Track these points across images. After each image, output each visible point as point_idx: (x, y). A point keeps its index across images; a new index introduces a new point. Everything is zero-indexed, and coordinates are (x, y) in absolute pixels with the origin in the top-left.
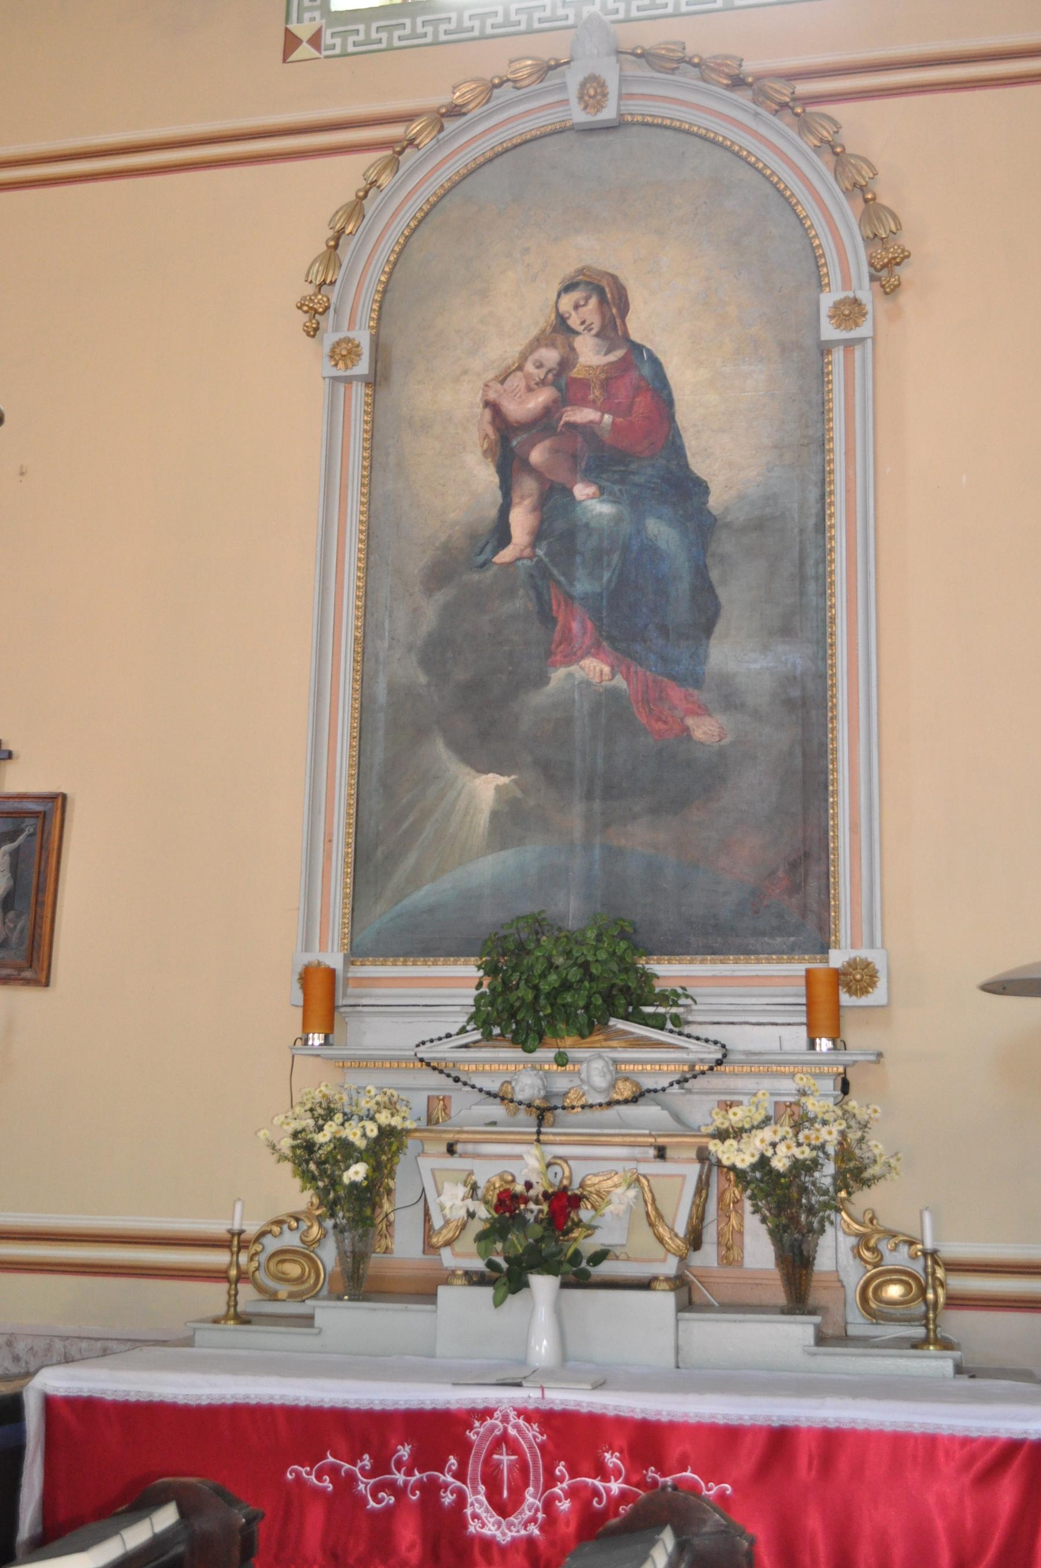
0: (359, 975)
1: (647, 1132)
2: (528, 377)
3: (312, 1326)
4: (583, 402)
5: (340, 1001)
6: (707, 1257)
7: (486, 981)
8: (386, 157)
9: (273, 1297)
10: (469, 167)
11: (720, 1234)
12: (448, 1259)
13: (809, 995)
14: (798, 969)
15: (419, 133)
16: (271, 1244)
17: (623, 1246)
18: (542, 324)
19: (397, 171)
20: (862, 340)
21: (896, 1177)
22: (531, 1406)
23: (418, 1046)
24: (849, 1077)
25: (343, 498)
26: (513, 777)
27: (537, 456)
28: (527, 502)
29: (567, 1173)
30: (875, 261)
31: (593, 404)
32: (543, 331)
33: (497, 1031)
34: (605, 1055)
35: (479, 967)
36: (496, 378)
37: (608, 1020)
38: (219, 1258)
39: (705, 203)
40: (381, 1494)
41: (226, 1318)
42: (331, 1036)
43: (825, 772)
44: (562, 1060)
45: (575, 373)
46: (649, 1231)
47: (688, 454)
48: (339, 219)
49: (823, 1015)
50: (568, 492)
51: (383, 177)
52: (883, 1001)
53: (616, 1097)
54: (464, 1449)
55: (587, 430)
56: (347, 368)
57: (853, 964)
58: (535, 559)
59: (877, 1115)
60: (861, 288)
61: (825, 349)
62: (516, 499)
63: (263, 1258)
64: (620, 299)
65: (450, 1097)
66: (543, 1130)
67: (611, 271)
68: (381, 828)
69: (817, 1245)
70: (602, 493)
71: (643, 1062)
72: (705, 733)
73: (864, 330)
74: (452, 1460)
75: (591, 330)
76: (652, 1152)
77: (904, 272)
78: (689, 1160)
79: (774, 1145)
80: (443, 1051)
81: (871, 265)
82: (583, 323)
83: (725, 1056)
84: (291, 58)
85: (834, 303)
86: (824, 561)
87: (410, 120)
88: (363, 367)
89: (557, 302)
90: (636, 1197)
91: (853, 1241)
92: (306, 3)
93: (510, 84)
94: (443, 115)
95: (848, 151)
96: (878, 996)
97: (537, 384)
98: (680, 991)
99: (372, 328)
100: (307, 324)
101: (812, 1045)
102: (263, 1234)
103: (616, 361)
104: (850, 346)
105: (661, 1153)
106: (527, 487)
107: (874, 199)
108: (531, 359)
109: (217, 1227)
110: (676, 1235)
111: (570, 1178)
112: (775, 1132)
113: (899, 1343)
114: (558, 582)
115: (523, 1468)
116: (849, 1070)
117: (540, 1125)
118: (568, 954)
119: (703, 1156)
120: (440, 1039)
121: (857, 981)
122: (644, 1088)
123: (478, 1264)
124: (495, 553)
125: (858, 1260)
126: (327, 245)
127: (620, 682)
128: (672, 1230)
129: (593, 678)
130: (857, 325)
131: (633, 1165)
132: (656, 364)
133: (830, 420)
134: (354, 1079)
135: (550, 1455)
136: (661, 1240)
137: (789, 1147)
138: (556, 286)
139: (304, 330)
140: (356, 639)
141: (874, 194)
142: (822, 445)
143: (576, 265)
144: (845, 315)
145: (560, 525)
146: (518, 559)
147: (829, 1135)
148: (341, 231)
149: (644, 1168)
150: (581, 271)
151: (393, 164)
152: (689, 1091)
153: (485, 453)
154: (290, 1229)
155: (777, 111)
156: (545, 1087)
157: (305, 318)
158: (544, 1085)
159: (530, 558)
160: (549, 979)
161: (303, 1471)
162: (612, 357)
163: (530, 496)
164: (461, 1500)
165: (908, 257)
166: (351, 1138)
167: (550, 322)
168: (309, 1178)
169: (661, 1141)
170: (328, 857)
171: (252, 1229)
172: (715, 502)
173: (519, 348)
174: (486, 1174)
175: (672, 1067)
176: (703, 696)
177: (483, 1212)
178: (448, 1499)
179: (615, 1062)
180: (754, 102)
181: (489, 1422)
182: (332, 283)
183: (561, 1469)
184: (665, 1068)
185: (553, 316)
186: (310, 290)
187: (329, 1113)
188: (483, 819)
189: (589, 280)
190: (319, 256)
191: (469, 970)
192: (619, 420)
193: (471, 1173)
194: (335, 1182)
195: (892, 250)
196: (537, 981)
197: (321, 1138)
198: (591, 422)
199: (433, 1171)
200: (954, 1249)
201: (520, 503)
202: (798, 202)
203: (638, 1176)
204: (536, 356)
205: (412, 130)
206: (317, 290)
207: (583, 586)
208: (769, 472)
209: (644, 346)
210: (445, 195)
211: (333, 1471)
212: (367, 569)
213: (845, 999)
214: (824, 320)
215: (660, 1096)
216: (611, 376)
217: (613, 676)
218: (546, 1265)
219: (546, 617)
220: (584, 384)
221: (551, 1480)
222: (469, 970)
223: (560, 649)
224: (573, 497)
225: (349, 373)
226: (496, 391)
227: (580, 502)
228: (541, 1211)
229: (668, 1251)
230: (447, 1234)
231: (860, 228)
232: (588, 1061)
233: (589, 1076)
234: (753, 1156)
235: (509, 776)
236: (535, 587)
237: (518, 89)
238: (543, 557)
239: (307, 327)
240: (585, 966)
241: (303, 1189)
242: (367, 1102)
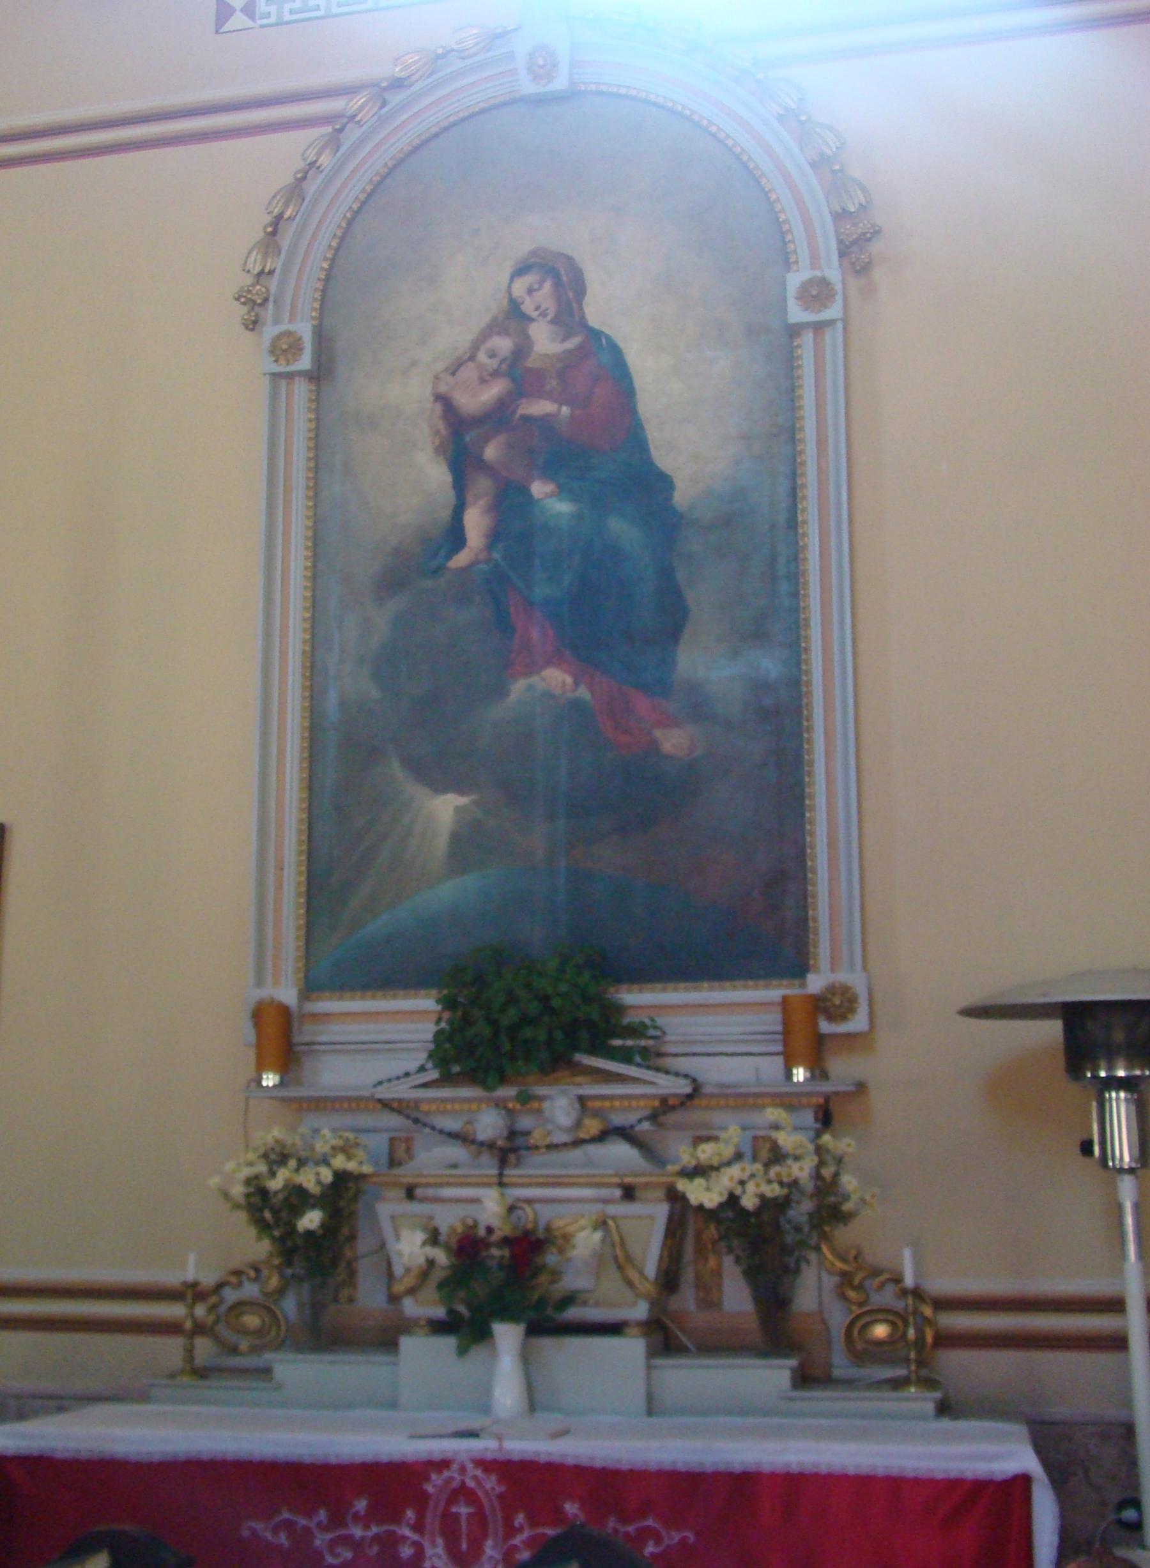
2: (481, 367)
3: (271, 1380)
5: (297, 1039)
6: (686, 1299)
7: (446, 1015)
9: (234, 1350)
10: (414, 144)
11: (698, 1276)
12: (410, 1307)
14: (774, 993)
16: (231, 1296)
19: (337, 151)
20: (832, 322)
22: (489, 1456)
23: (375, 1086)
25: (287, 502)
27: (491, 452)
32: (495, 319)
33: (456, 1069)
35: (438, 1001)
36: (446, 370)
38: (174, 1311)
40: (339, 1550)
41: (182, 1372)
45: (531, 363)
46: (618, 1275)
47: (652, 447)
48: (277, 204)
50: (524, 491)
53: (582, 1135)
54: (421, 1501)
55: (545, 423)
57: (831, 990)
62: (469, 498)
63: (223, 1309)
66: (507, 1172)
71: (611, 1098)
73: (834, 311)
74: (410, 1514)
76: (618, 1193)
79: (742, 1183)
80: (401, 1091)
82: (537, 309)
86: (796, 559)
88: (305, 362)
89: (509, 287)
90: (603, 1241)
91: (836, 1279)
94: (385, 89)
96: (858, 1023)
98: (647, 1021)
99: (313, 318)
100: (245, 317)
101: (789, 1075)
102: (220, 1286)
105: (629, 1193)
106: (482, 487)
108: (483, 348)
109: (172, 1278)
110: (646, 1279)
112: (743, 1170)
113: (880, 1384)
115: (480, 1518)
118: (528, 985)
119: (675, 1197)
123: (440, 1312)
124: (449, 556)
126: (265, 232)
127: (584, 693)
130: (826, 307)
131: (599, 1207)
133: (801, 408)
134: (312, 1120)
135: (508, 1505)
136: (630, 1284)
137: (758, 1185)
139: (244, 324)
140: (304, 652)
147: (802, 1170)
148: (279, 217)
149: (611, 1209)
150: (534, 253)
152: (661, 1126)
154: (249, 1279)
157: (244, 309)
161: (259, 1526)
162: (570, 344)
164: (419, 1554)
166: (306, 1185)
168: (263, 1227)
170: (279, 886)
171: (209, 1279)
172: (681, 498)
174: (448, 1219)
175: (642, 1103)
177: (441, 1256)
178: (406, 1552)
179: (582, 1099)
181: (446, 1474)
182: (271, 272)
183: (520, 1519)
184: (634, 1103)
185: (505, 302)
186: (249, 280)
187: (283, 1159)
188: (441, 844)
191: (427, 1003)
192: (578, 412)
194: (291, 1231)
195: (861, 225)
197: (275, 1184)
198: (548, 415)
199: (393, 1217)
200: (942, 1284)
205: (353, 106)
207: (542, 591)
211: (288, 1525)
212: (315, 577)
213: (825, 1027)
216: (569, 364)
218: (507, 1314)
219: (503, 624)
220: (539, 375)
221: (511, 1531)
222: (427, 1003)
224: (531, 496)
227: (539, 500)
228: (503, 1257)
229: (637, 1295)
230: (409, 1282)
239: (245, 319)
240: (545, 999)
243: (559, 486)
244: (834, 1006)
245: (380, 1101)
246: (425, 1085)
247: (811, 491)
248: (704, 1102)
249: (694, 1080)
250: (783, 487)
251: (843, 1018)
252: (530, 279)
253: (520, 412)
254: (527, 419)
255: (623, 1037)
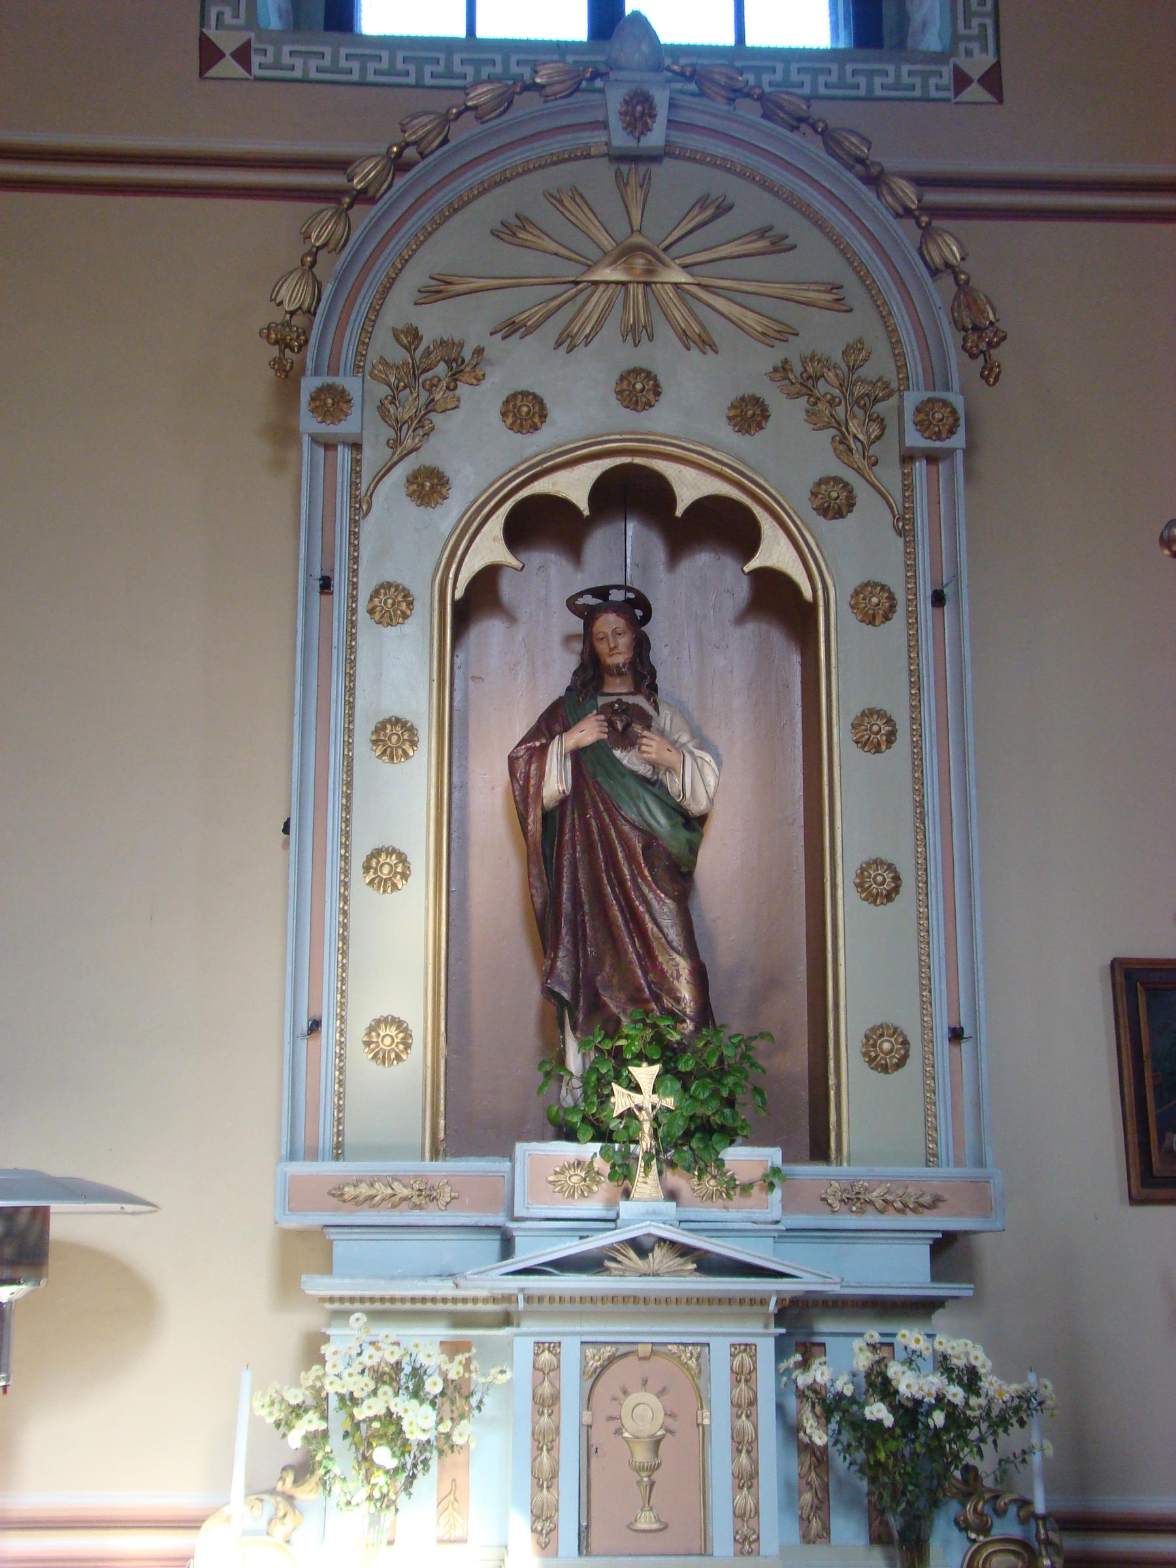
20: (950, 452)
92: (974, 5)
214: (909, 426)
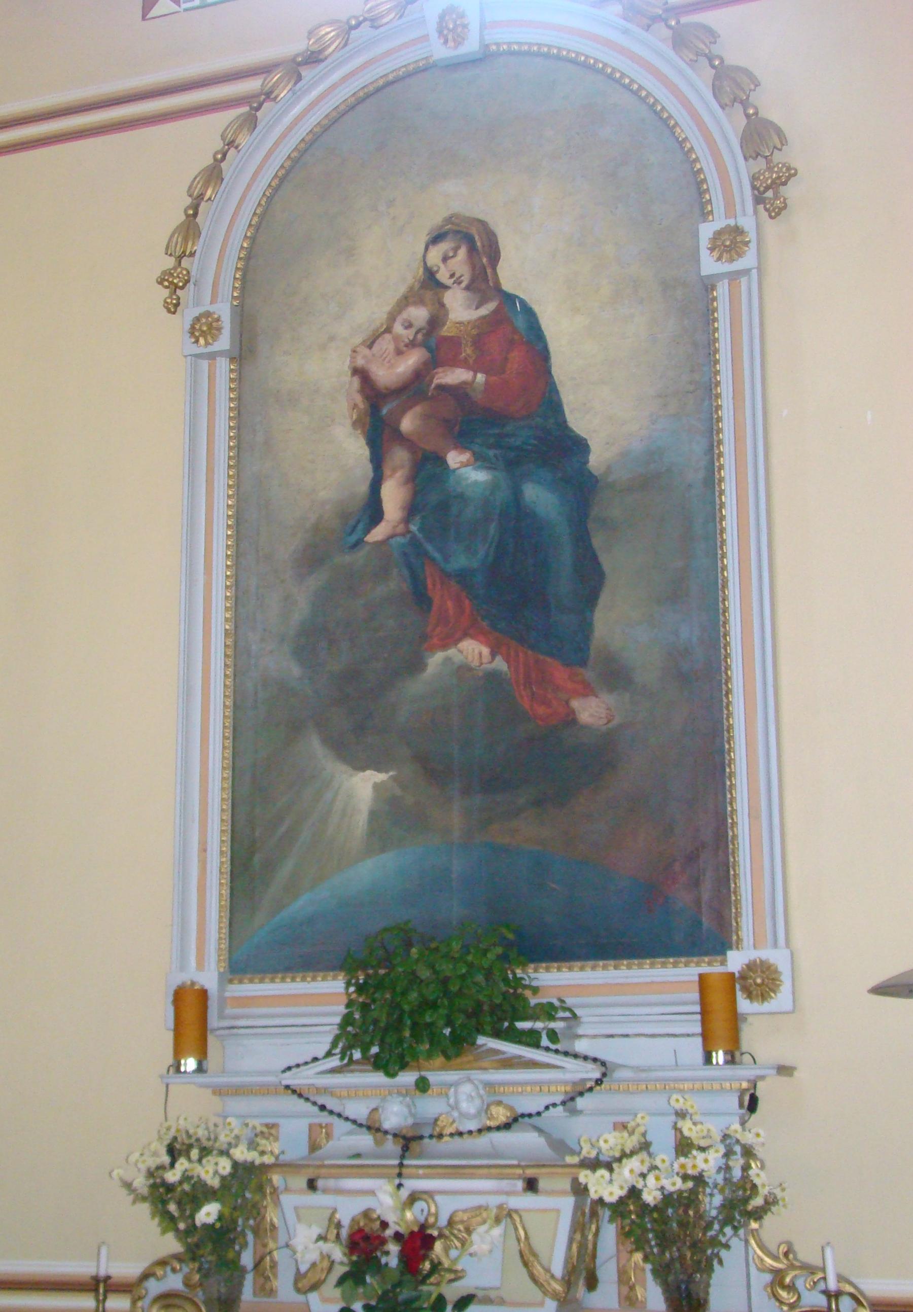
0: (237, 994)
1: (515, 1162)
2: (396, 339)
4: (454, 362)
8: (242, 115)
13: (703, 1002)
15: (276, 85)
16: (154, 1287)
17: (497, 1289)
18: (410, 280)
19: (255, 128)
20: (746, 272)
21: (783, 1210)
23: (284, 1071)
24: (758, 1094)
26: (391, 773)
27: (407, 424)
28: (399, 474)
29: (433, 1210)
30: (757, 184)
31: (465, 364)
32: (411, 289)
34: (473, 1077)
36: (363, 343)
37: (475, 1039)
39: (578, 134)
42: (205, 1063)
43: (721, 752)
44: (422, 1086)
45: (446, 331)
49: (719, 1025)
50: (440, 460)
51: (240, 136)
52: (788, 1006)
55: (458, 393)
56: (207, 344)
57: (751, 967)
58: (408, 536)
59: (761, 1140)
60: (744, 214)
61: (709, 285)
62: (387, 472)
64: (490, 246)
65: (332, 1124)
66: (406, 1162)
67: (481, 217)
68: (257, 834)
69: (708, 1285)
70: (476, 460)
72: (592, 715)
73: (748, 260)
75: (460, 283)
76: (520, 1185)
77: (791, 191)
78: (563, 1193)
79: (643, 1176)
80: (300, 1079)
81: (754, 188)
82: (452, 276)
83: (604, 1075)
84: (151, 15)
85: (714, 233)
87: (267, 72)
88: (224, 342)
89: (424, 256)
91: (768, 1277)
93: (368, 23)
94: (299, 64)
95: (727, 62)
96: (781, 1000)
97: (406, 346)
98: (557, 1003)
101: (708, 1059)
103: (488, 315)
104: (735, 279)
106: (399, 457)
107: (756, 113)
110: (553, 1276)
111: (436, 1216)
112: (642, 1162)
114: (433, 560)
116: (760, 1085)
117: (403, 1157)
120: (306, 1063)
121: (758, 985)
122: (520, 1110)
124: (368, 531)
125: (773, 1300)
127: (500, 664)
128: (547, 1270)
129: (472, 661)
130: (740, 255)
132: (529, 313)
138: (424, 238)
141: (756, 108)
142: (710, 389)
143: (445, 214)
144: (725, 246)
145: (433, 498)
146: (392, 536)
150: (449, 220)
151: (250, 122)
153: (355, 424)
155: (649, 26)
156: (412, 1115)
157: (166, 293)
158: (410, 1111)
159: (403, 535)
160: (409, 998)
162: (485, 311)
163: (402, 467)
165: (795, 174)
167: (418, 278)
168: (169, 1221)
169: (530, 1172)
172: (597, 460)
173: (387, 309)
176: (589, 674)
177: (338, 1253)
179: (490, 1086)
180: (625, 19)
182: (192, 254)
185: (421, 270)
188: (361, 820)
189: (455, 228)
190: (177, 228)
192: (494, 379)
193: (335, 1211)
195: (776, 169)
196: (399, 999)
198: (465, 383)
199: (296, 1209)
201: (391, 476)
202: (676, 124)
203: (509, 1211)
204: (404, 315)
205: (268, 83)
206: (177, 264)
208: (653, 424)
209: (517, 297)
210: (306, 150)
214: (704, 254)
215: (535, 1120)
217: (493, 658)
220: (454, 342)
223: (438, 630)
225: (210, 349)
226: (364, 357)
227: (454, 470)
231: (742, 147)
232: (456, 1084)
233: (457, 1102)
234: (621, 1188)
235: (387, 772)
236: (409, 566)
237: (377, 28)
238: (417, 532)
241: (164, 1232)
242: (226, 1135)
243: (474, 453)
244: (756, 984)
245: (287, 1087)
246: (333, 1071)
247: (728, 448)
248: (615, 1086)
249: (603, 1064)
250: (698, 447)
251: (764, 997)
252: (444, 247)
253: (436, 381)
254: (441, 388)
255: (534, 1018)
